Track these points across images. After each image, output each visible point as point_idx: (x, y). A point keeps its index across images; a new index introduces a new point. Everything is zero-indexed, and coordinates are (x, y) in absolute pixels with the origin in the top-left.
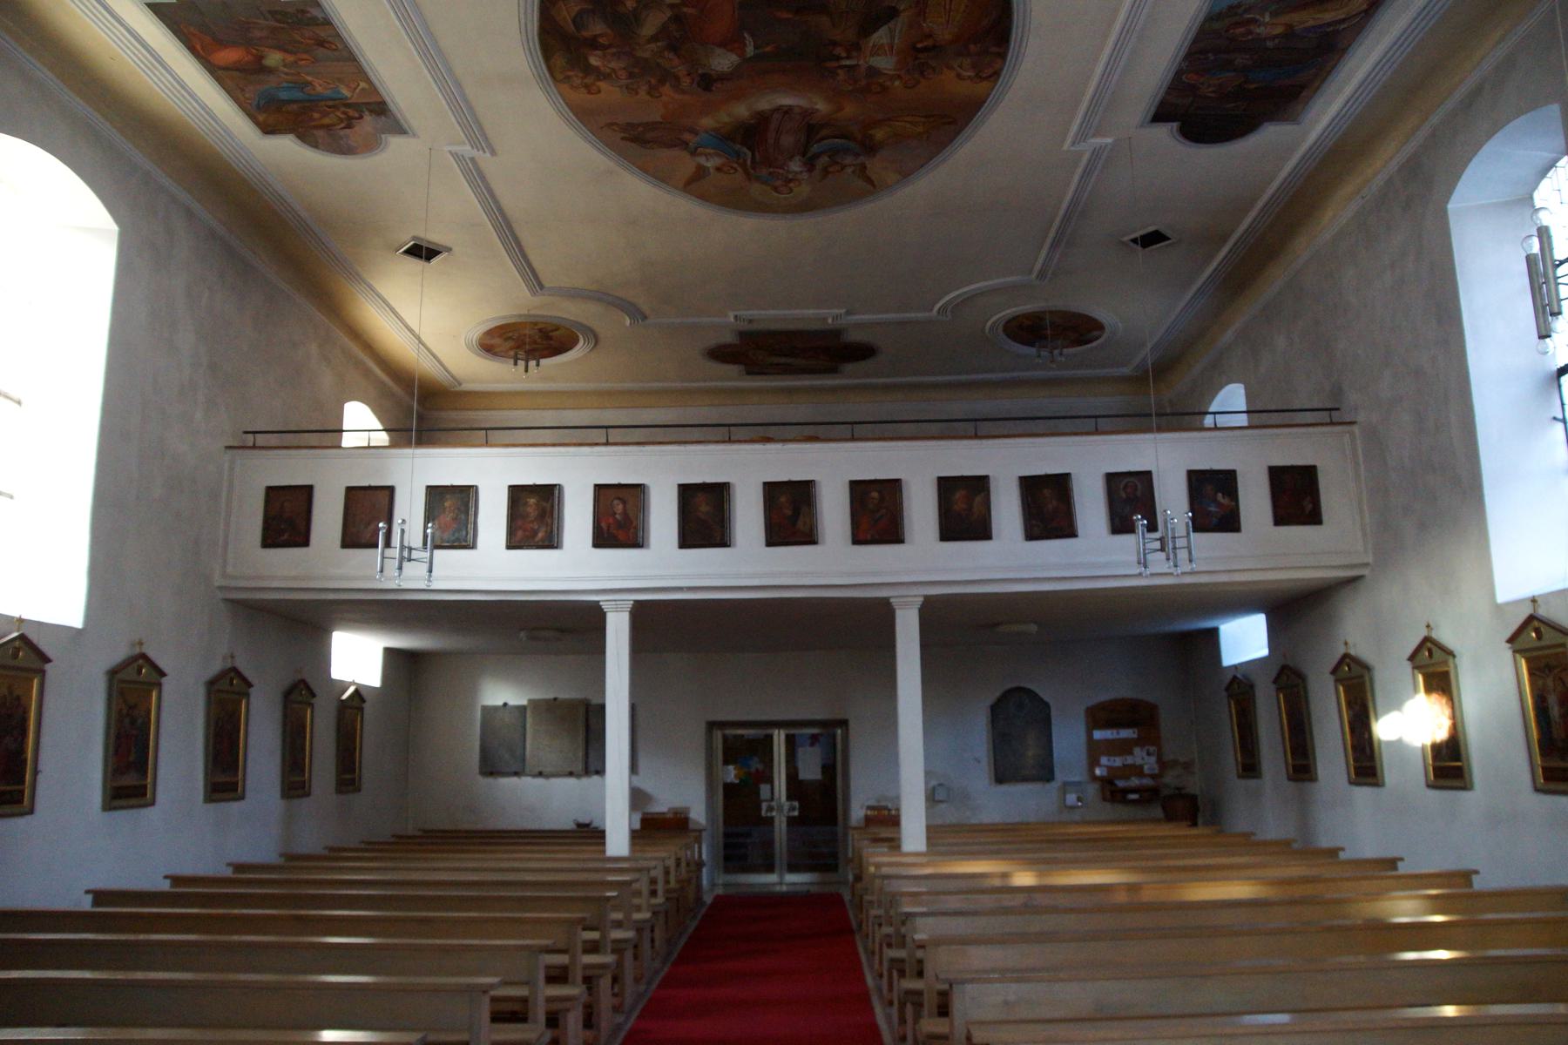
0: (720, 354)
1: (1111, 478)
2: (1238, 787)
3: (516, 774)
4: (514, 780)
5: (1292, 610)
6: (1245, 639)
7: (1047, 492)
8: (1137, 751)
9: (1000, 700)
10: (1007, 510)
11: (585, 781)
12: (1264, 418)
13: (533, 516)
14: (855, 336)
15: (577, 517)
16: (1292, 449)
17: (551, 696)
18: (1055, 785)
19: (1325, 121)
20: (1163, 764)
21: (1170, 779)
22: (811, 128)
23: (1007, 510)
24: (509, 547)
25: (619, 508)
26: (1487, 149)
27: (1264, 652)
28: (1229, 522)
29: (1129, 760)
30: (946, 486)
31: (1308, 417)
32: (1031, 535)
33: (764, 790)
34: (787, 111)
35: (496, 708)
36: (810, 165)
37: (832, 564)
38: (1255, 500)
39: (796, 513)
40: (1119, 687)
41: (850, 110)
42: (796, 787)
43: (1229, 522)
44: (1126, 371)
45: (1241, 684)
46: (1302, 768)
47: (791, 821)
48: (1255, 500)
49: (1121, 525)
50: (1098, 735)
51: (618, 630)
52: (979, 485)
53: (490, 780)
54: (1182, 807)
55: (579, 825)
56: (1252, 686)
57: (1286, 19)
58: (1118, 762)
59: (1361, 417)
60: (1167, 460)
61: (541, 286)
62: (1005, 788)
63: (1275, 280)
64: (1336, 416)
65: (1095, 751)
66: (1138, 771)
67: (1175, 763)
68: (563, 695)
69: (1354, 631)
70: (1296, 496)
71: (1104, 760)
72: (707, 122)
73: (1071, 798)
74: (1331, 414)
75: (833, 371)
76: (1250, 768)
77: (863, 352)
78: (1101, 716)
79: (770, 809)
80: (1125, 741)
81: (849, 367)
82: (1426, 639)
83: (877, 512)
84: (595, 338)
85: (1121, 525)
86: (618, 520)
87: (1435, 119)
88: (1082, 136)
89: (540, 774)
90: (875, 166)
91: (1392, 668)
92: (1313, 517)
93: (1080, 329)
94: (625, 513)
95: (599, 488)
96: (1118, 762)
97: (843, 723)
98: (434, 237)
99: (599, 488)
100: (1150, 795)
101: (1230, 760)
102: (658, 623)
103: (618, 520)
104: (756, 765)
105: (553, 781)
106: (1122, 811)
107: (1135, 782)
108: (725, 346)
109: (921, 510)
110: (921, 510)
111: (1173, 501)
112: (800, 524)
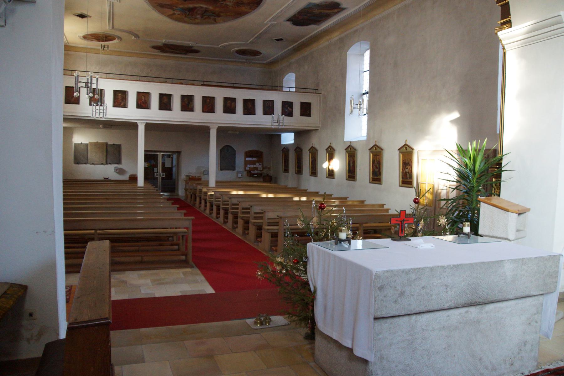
0: (155, 47)
1: (264, 101)
2: (282, 175)
3: (85, 163)
4: (85, 165)
5: (300, 134)
6: (288, 139)
7: (249, 103)
8: (257, 164)
9: (223, 148)
10: (239, 107)
11: (106, 166)
12: (300, 90)
13: (120, 99)
14: (195, 48)
15: (132, 100)
16: (306, 99)
17: (96, 141)
18: (235, 172)
19: (325, 26)
20: (263, 168)
21: (265, 171)
22: (206, 11)
23: (239, 107)
24: (114, 107)
25: (143, 98)
26: (356, 44)
27: (292, 142)
28: (290, 114)
29: (255, 166)
30: (226, 99)
31: (311, 91)
32: (245, 114)
33: (155, 169)
34: (202, 8)
35: (79, 144)
36: (202, 17)
37: (197, 117)
38: (297, 110)
39: (189, 103)
40: (253, 147)
41: (217, 9)
42: (164, 169)
43: (290, 114)
44: (265, 62)
45: (286, 149)
46: (299, 171)
47: (163, 178)
48: (297, 110)
49: (266, 113)
50: (247, 159)
51: (141, 130)
52: (233, 100)
53: (77, 165)
54: (267, 179)
55: (105, 178)
56: (288, 150)
57: (320, 11)
58: (252, 166)
59: (323, 93)
60: (277, 98)
61: (113, 28)
62: (223, 172)
63: (307, 52)
64: (317, 91)
65: (246, 163)
66: (257, 169)
67: (266, 168)
68: (99, 141)
69: (315, 141)
70: (306, 109)
71: (248, 166)
72: (182, 6)
73: (240, 175)
74: (316, 91)
75: (186, 54)
76: (286, 170)
77: (196, 51)
78: (249, 154)
79: (157, 175)
80: (254, 161)
81: (190, 54)
82: (330, 146)
83: (208, 105)
84: (120, 38)
85: (266, 113)
86: (143, 101)
87: (348, 32)
88: (270, 21)
89: (93, 164)
90: (218, 19)
91: (322, 154)
92: (309, 115)
93: (255, 53)
94: (145, 100)
95: (138, 93)
96: (252, 166)
97: (179, 153)
98: (85, 12)
99: (138, 93)
100: (260, 175)
101: (281, 167)
102: (150, 127)
103: (143, 101)
104: (153, 162)
105: (96, 166)
106: (253, 179)
107: (256, 172)
108: (160, 46)
109: (219, 105)
110: (219, 105)
111: (278, 108)
112: (190, 107)
